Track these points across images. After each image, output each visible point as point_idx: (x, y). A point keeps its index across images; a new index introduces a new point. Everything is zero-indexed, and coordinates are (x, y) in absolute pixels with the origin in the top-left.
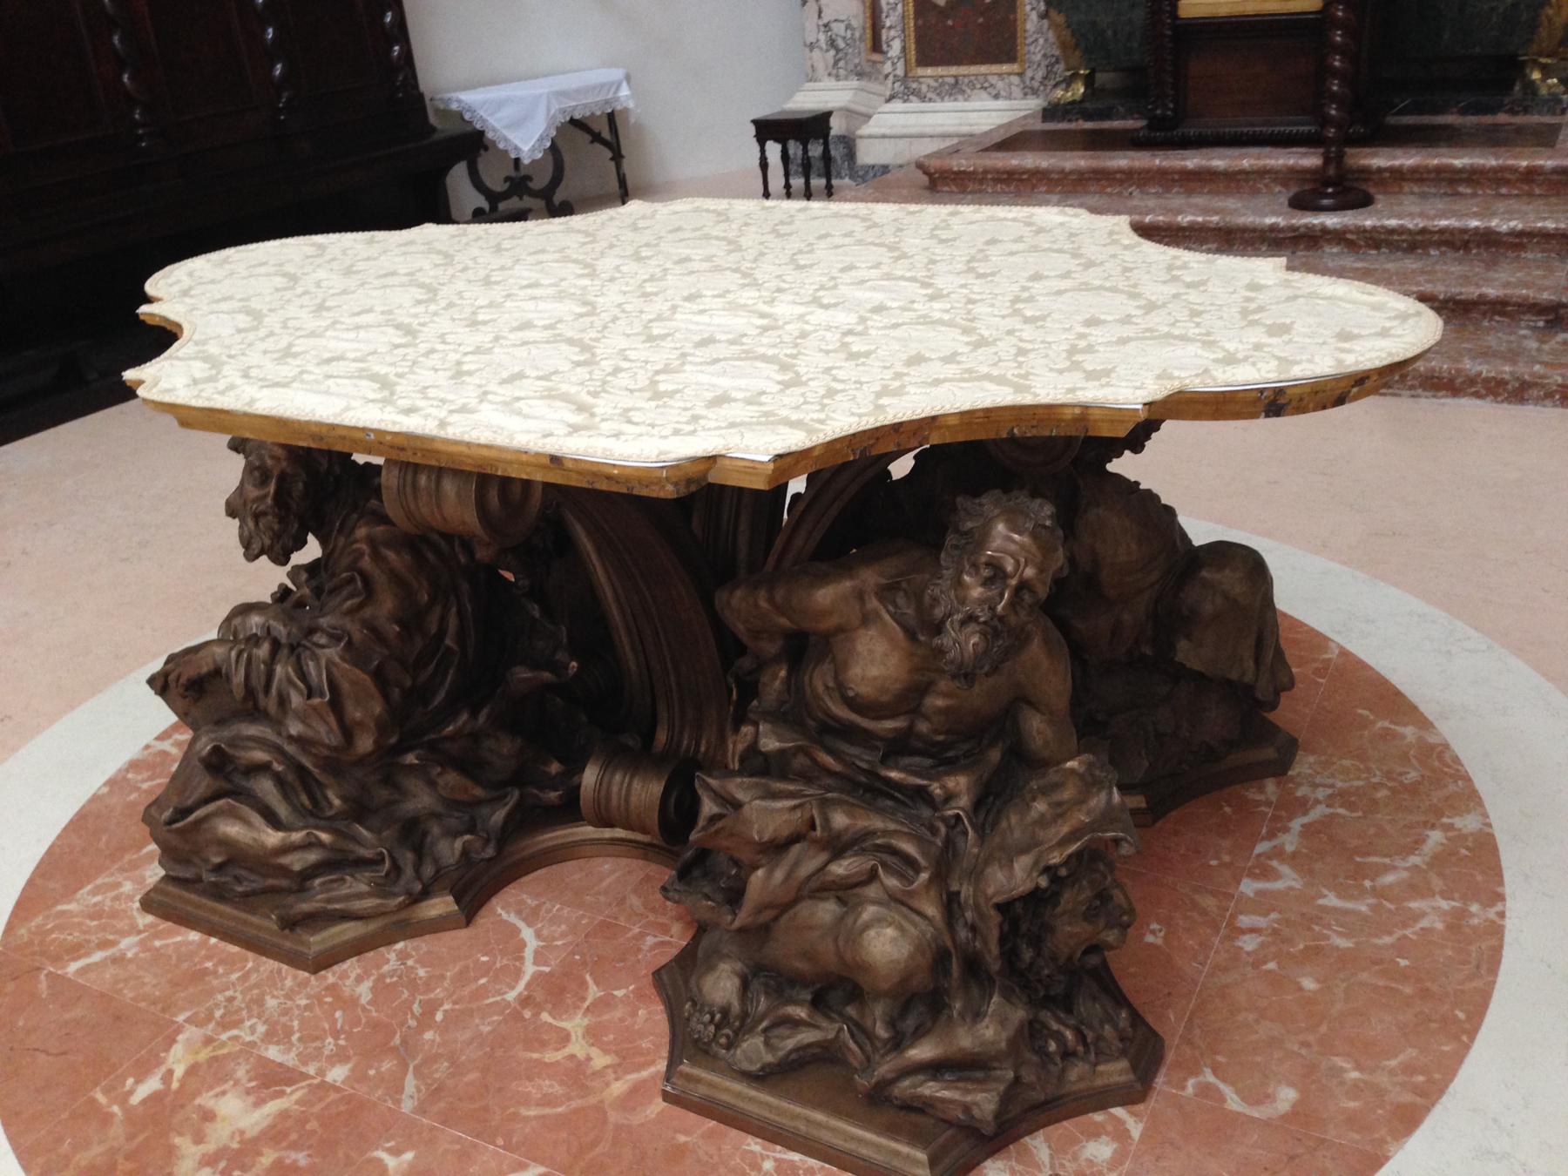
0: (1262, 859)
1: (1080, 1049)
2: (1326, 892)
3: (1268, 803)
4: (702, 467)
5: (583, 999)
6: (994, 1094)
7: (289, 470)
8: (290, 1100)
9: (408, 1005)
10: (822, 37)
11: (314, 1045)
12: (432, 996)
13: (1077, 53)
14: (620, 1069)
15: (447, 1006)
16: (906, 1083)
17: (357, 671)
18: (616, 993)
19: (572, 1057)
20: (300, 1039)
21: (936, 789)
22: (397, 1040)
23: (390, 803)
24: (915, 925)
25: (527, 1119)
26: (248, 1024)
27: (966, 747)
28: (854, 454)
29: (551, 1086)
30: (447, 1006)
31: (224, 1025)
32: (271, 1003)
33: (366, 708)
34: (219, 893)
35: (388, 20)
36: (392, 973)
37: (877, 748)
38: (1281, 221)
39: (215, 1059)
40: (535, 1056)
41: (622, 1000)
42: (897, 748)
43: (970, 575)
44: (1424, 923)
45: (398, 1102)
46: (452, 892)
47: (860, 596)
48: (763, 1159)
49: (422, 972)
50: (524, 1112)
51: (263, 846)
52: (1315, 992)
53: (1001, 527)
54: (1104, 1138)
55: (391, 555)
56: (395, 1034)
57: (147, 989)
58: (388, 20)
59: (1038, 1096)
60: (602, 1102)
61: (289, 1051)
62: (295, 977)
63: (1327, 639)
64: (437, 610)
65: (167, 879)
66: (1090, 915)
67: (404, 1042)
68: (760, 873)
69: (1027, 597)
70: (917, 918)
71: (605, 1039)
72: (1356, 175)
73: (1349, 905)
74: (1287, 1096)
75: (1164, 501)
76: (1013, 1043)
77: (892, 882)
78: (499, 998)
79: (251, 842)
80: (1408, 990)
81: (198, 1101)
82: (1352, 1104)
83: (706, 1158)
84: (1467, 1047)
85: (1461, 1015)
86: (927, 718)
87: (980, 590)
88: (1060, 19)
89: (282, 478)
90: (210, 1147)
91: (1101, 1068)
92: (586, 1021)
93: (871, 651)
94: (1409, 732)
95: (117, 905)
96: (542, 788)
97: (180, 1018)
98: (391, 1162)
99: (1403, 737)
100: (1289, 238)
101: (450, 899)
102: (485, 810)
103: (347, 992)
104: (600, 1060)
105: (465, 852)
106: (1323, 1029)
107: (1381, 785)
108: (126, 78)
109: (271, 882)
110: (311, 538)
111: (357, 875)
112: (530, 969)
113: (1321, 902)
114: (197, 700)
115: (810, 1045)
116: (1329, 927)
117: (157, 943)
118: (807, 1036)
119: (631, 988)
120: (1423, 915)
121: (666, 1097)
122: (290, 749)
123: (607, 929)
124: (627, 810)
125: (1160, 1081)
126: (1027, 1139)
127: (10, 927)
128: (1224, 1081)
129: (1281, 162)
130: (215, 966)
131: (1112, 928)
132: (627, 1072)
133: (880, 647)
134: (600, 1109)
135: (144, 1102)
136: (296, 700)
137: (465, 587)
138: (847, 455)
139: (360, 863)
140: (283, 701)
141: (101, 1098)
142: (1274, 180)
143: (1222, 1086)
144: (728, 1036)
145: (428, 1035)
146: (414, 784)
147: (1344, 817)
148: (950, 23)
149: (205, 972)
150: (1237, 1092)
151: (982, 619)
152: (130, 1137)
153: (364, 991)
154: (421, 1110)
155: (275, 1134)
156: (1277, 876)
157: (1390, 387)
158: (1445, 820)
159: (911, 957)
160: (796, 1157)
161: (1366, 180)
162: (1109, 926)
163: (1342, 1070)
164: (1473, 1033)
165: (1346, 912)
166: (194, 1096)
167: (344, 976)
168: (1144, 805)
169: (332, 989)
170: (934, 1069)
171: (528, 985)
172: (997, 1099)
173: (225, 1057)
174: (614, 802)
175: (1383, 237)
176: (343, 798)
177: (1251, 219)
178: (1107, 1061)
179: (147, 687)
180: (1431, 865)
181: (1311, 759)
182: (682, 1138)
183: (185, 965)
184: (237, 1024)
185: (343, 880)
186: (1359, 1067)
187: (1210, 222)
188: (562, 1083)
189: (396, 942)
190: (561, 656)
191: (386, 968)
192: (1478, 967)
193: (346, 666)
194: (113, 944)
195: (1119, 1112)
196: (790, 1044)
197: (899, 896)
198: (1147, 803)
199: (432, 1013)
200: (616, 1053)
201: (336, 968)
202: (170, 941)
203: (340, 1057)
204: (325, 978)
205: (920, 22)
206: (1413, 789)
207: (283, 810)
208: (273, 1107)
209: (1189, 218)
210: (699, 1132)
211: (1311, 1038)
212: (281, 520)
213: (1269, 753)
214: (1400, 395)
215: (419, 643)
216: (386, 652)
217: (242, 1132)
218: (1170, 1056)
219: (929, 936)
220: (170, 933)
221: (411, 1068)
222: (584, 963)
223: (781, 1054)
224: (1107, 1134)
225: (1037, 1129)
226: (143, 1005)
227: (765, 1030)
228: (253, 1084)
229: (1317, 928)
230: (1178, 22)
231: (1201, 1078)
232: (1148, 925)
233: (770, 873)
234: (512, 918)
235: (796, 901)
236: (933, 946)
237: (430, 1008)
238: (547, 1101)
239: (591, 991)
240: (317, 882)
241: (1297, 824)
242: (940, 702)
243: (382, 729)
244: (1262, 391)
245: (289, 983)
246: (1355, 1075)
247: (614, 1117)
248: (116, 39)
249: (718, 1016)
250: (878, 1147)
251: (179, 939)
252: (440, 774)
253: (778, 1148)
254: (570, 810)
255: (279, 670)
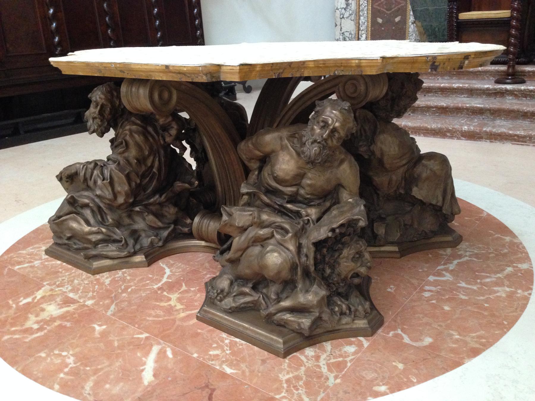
0: (440, 271)
1: (348, 311)
2: (461, 282)
3: (446, 255)
4: (216, 68)
5: (180, 290)
6: (310, 320)
7: (105, 103)
8: (71, 308)
9: (121, 286)
10: (341, 37)
11: (85, 294)
12: (129, 284)
13: (425, 36)
14: (184, 310)
15: (133, 288)
16: (279, 314)
17: (120, 174)
18: (191, 289)
19: (170, 305)
20: (81, 292)
21: (303, 212)
22: (113, 295)
23: (130, 225)
24: (285, 253)
25: (148, 320)
26: (66, 286)
27: (318, 202)
28: (275, 76)
29: (160, 312)
30: (133, 288)
31: (58, 286)
32: (76, 282)
33: (122, 187)
34: (68, 247)
35: (197, 23)
36: (118, 277)
37: (285, 199)
38: (491, 87)
39: (52, 295)
40: (158, 303)
41: (193, 291)
42: (293, 199)
43: (316, 126)
44: (498, 294)
45: (106, 312)
46: (144, 254)
47: (281, 138)
48: (226, 340)
49: (128, 278)
50: (148, 318)
51: (83, 231)
52: (448, 311)
53: (329, 109)
54: (353, 346)
55: (136, 136)
56: (113, 293)
57: (38, 275)
58: (197, 23)
59: (329, 327)
60: (175, 318)
61: (76, 295)
62: (86, 275)
63: (483, 210)
64: (151, 158)
65: (56, 244)
66: (354, 259)
67: (115, 296)
68: (237, 238)
69: (337, 135)
70: (287, 251)
71: (183, 301)
72: (520, 74)
73: (469, 287)
74: (428, 340)
75: (417, 144)
76: (320, 302)
77: (278, 237)
78: (151, 287)
79: (79, 229)
80: (486, 313)
81: (42, 306)
82: (454, 346)
83: (206, 337)
84: (506, 333)
85: (505, 323)
86: (303, 188)
87: (319, 131)
88: (419, 24)
89: (102, 106)
90: (39, 319)
91: (356, 322)
92: (178, 296)
93: (283, 159)
94: (508, 239)
95: (38, 253)
96: (183, 226)
97: (45, 283)
98: (97, 328)
99: (505, 239)
100: (493, 93)
101: (144, 256)
102: (162, 232)
103: (102, 281)
104: (179, 306)
105: (152, 243)
106: (449, 322)
107: (492, 253)
108: (109, 31)
109: (85, 245)
110: (111, 129)
111: (113, 245)
112: (165, 280)
113: (459, 285)
114: (71, 183)
115: (249, 302)
116: (460, 292)
117: (46, 263)
118: (248, 299)
119: (197, 288)
120: (498, 292)
121: (198, 318)
122: (97, 200)
123: (195, 272)
124: (208, 231)
125: (380, 331)
126: (324, 343)
127: (2, 255)
128: (405, 333)
129: (493, 68)
130: (62, 270)
131: (363, 266)
132: (187, 311)
133: (287, 158)
134: (174, 320)
135: (24, 304)
136: (99, 182)
137: (162, 152)
138: (272, 75)
139: (115, 241)
140: (95, 182)
141: (11, 302)
142: (491, 75)
143: (403, 335)
144: (221, 297)
145: (124, 295)
146: (138, 219)
147: (475, 261)
148: (383, 29)
149: (59, 272)
150: (409, 337)
151: (318, 141)
152: (15, 313)
153: (107, 281)
154: (113, 315)
155: (62, 317)
156: (444, 276)
157: (526, 142)
158: (515, 265)
159: (282, 263)
160: (238, 340)
161: (524, 75)
162: (361, 265)
163: (453, 335)
164: (508, 330)
165: (468, 288)
166: (41, 304)
167: (103, 276)
168: (397, 250)
169: (97, 280)
170: (292, 310)
171: (162, 285)
172: (310, 321)
173: (55, 295)
174: (204, 229)
175: (528, 93)
176: (113, 219)
177: (479, 86)
178: (358, 320)
179: (56, 178)
180: (505, 277)
181: (467, 244)
182: (199, 331)
183: (53, 270)
184: (62, 286)
185: (108, 246)
186: (459, 334)
187: (465, 86)
188: (164, 312)
189: (123, 269)
190: (193, 180)
191: (117, 276)
192: (516, 309)
193: (117, 171)
194: (32, 262)
195: (361, 339)
196: (242, 301)
197: (280, 242)
198: (399, 249)
199: (128, 289)
200: (186, 305)
201: (101, 274)
202: (51, 263)
203: (93, 298)
204: (96, 276)
205: (373, 28)
206: (505, 255)
207: (92, 221)
208: (65, 309)
209: (457, 85)
210: (206, 330)
211: (443, 324)
212: (101, 121)
213: (449, 238)
214: (529, 145)
215: (144, 168)
216: (131, 169)
217: (52, 315)
218: (386, 324)
219: (290, 257)
220: (51, 261)
221: (115, 303)
222: (183, 280)
223: (238, 304)
224: (355, 344)
225: (329, 340)
226: (35, 279)
227: (235, 296)
228: (61, 303)
229: (455, 292)
230: (459, 21)
231: (396, 332)
232: (389, 286)
233: (240, 239)
234: (164, 266)
235: (247, 248)
236: (291, 261)
237: (127, 288)
238: (157, 316)
239: (183, 288)
240: (100, 245)
241: (455, 262)
242: (309, 182)
243: (127, 195)
244: (427, 57)
245: (84, 277)
246: (457, 337)
247: (178, 323)
248: (107, 19)
249: (219, 291)
250: (266, 337)
251: (54, 262)
252: (147, 216)
253: (232, 337)
254: (190, 235)
255: (95, 172)
